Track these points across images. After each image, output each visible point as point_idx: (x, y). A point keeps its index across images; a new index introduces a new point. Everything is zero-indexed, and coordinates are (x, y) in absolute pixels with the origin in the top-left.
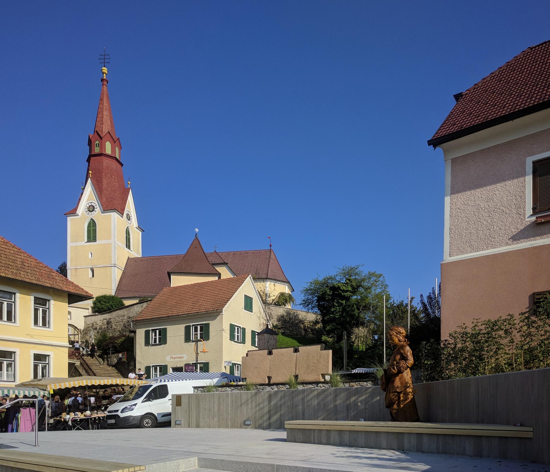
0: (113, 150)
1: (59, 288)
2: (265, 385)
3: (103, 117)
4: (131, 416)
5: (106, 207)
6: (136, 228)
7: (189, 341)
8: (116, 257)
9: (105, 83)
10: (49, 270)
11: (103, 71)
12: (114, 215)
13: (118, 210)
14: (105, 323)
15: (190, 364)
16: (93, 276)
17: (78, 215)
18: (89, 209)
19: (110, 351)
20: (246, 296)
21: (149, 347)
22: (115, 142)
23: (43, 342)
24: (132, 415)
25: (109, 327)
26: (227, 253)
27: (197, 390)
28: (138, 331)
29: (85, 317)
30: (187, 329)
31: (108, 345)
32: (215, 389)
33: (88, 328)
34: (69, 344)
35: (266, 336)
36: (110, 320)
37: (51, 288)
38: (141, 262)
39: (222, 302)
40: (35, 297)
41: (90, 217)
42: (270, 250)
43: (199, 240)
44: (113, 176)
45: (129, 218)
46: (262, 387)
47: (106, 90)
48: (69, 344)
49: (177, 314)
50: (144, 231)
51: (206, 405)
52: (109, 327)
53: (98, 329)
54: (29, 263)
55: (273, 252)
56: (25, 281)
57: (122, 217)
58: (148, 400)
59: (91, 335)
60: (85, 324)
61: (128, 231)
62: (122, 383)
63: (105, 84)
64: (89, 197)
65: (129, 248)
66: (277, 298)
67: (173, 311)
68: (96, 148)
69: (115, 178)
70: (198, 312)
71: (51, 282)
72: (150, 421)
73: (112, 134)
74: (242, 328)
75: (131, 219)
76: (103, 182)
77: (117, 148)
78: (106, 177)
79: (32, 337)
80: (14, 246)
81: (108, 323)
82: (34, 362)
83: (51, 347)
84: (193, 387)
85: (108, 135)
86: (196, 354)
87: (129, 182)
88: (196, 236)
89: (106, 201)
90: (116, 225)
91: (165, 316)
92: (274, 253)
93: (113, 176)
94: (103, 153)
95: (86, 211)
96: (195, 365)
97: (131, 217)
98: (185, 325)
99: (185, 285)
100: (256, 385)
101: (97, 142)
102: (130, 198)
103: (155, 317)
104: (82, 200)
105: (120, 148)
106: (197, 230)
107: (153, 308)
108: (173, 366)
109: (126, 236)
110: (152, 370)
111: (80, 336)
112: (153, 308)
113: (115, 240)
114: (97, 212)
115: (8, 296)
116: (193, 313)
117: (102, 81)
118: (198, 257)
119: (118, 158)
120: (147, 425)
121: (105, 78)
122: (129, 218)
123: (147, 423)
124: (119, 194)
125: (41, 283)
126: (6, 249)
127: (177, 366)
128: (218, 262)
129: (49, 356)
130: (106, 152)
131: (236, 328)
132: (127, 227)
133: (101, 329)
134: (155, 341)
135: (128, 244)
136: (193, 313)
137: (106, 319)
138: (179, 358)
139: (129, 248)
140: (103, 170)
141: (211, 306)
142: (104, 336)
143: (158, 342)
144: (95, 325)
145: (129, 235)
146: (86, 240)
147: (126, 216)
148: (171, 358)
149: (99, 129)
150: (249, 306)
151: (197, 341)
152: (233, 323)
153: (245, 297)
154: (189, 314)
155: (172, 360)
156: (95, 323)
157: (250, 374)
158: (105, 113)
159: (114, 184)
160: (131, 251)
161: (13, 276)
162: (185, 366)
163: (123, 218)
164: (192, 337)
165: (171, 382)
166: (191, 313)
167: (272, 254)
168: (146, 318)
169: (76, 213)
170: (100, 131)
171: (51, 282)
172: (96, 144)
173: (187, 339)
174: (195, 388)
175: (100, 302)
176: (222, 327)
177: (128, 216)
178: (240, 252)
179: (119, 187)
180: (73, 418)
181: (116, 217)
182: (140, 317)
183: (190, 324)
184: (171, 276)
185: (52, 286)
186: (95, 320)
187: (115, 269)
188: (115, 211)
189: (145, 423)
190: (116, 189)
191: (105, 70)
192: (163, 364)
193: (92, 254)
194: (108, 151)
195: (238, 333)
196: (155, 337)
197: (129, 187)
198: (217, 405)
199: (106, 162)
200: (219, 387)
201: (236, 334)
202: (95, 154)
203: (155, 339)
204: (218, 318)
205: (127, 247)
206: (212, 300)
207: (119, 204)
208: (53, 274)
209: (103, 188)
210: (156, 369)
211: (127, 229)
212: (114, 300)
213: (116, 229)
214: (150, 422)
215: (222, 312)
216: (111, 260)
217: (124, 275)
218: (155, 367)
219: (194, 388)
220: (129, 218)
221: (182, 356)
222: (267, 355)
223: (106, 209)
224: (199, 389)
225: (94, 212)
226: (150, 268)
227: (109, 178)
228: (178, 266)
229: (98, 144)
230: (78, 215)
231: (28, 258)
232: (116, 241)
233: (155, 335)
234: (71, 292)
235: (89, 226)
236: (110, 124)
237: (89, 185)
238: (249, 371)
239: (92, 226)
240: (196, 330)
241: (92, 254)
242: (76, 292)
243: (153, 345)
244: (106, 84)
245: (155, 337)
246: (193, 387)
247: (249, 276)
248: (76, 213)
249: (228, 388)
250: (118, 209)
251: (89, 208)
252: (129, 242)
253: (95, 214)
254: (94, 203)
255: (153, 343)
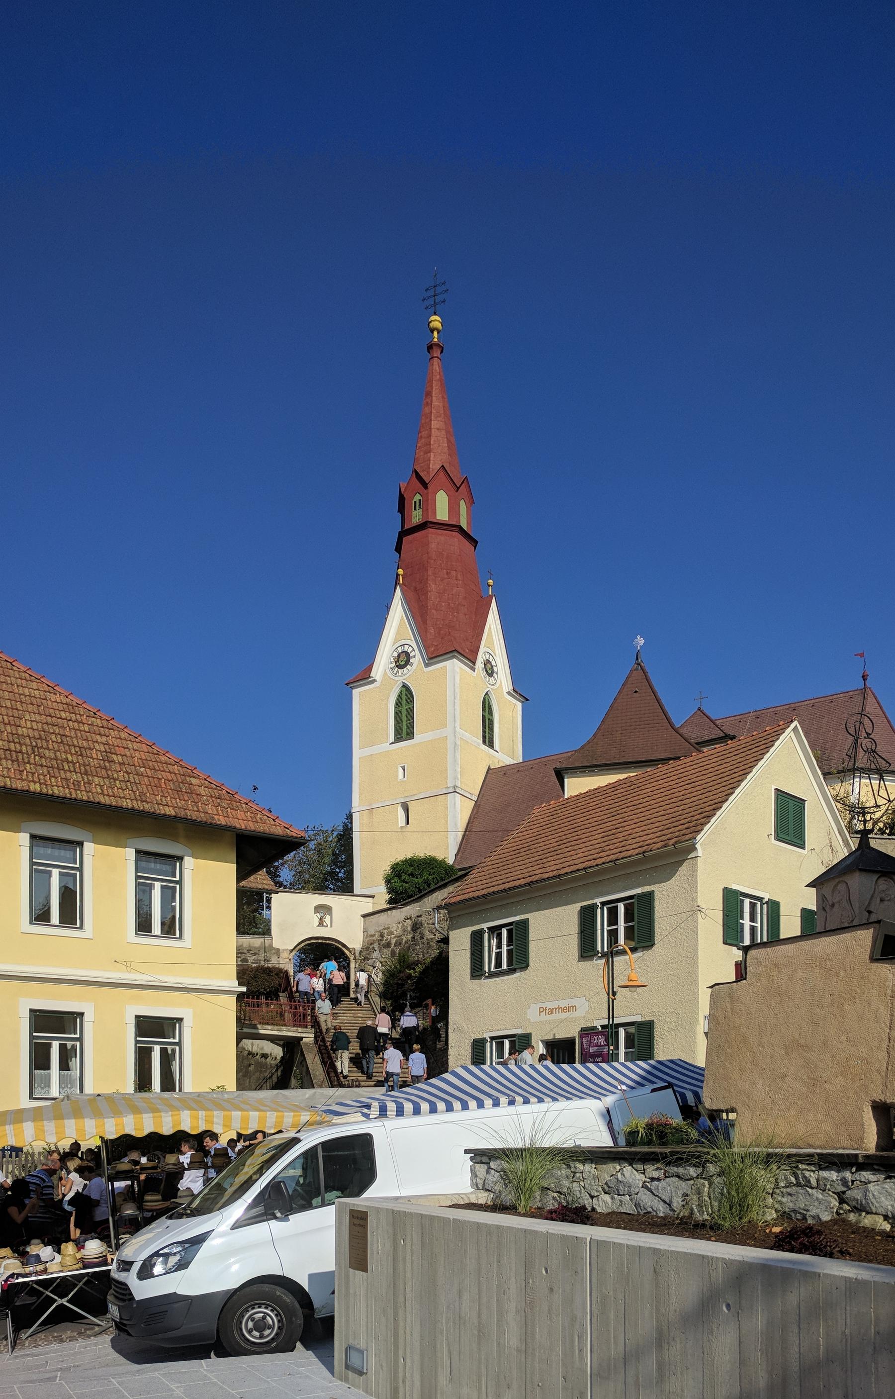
0: (453, 509)
1: (202, 817)
2: (861, 1167)
3: (430, 436)
4: (173, 1298)
5: (434, 650)
6: (509, 693)
7: (592, 953)
8: (459, 770)
9: (436, 352)
10: (182, 771)
11: (431, 324)
12: (454, 666)
13: (462, 653)
14: (409, 929)
15: (595, 1028)
16: (408, 823)
17: (375, 681)
18: (398, 664)
19: (406, 1000)
20: (780, 794)
21: (483, 981)
22: (455, 488)
23: (161, 981)
24: (182, 1291)
25: (416, 938)
26: (736, 718)
27: (486, 1167)
28: (454, 935)
29: (364, 916)
30: (587, 917)
31: (403, 985)
32: (564, 1172)
33: (371, 944)
34: (240, 985)
35: (857, 882)
36: (420, 919)
37: (176, 818)
38: (518, 775)
39: (694, 818)
40: (138, 852)
41: (400, 680)
42: (864, 691)
43: (647, 669)
44: (454, 573)
45: (489, 670)
46: (833, 1175)
47: (438, 369)
48: (240, 985)
49: (555, 873)
50: (527, 700)
51: (466, 1296)
52: (417, 937)
53: (393, 946)
54: (128, 754)
55: (873, 694)
56: (98, 803)
57: (473, 669)
58: (265, 1214)
59: (375, 961)
60: (364, 935)
61: (489, 704)
62: (202, 1127)
63: (435, 356)
64: (398, 633)
65: (491, 745)
66: (890, 812)
67: (547, 865)
68: (414, 513)
69: (456, 577)
70: (616, 860)
71: (181, 803)
72: (272, 1319)
73: (450, 471)
74: (767, 902)
75: (497, 673)
76: (430, 592)
77: (462, 503)
78: (436, 577)
79: (128, 966)
80: (95, 714)
81: (416, 927)
82: (137, 1042)
83: (185, 995)
84: (467, 1151)
85: (442, 474)
86: (608, 994)
87: (491, 582)
88: (637, 659)
89: (437, 635)
90: (458, 690)
91: (522, 882)
92: (876, 698)
93: (454, 573)
94: (430, 520)
95: (392, 669)
96: (610, 1031)
97: (495, 669)
98: (578, 906)
99: (590, 791)
100: (793, 1160)
101: (418, 497)
102: (493, 622)
103: (496, 889)
104: (384, 643)
105: (471, 502)
106: (640, 641)
107: (496, 866)
108: (546, 1037)
109: (484, 717)
110: (490, 1050)
111: (354, 966)
112: (496, 866)
113: (455, 727)
114: (414, 666)
115: (69, 854)
116: (603, 863)
117: (429, 352)
118: (642, 716)
119: (465, 527)
120: (257, 1334)
121: (436, 340)
122: (490, 672)
123: (260, 1326)
124: (466, 615)
125: (147, 807)
126: (70, 720)
127: (557, 1037)
128: (707, 738)
129: (180, 1020)
130: (437, 518)
131: (747, 902)
132: (487, 694)
133: (400, 944)
134: (498, 964)
135: (487, 735)
136: (603, 863)
137: (410, 918)
138: (563, 1010)
139: (491, 745)
140: (429, 561)
141: (658, 834)
142: (404, 962)
143: (505, 966)
144: (385, 935)
145: (491, 713)
146: (392, 739)
147: (483, 666)
148: (542, 1010)
149: (422, 465)
150: (791, 826)
151: (611, 954)
152: (735, 887)
153: (777, 798)
154: (591, 867)
155: (544, 1017)
156: (385, 931)
157: (760, 1086)
158: (435, 424)
159: (455, 591)
160: (496, 751)
161: (67, 790)
162: (581, 1037)
163: (474, 671)
164: (601, 943)
165: (392, 1123)
166: (597, 865)
167: (870, 700)
168: (471, 895)
169: (370, 677)
170: (423, 471)
171: (181, 803)
172: (415, 502)
173: (587, 950)
174: (478, 1159)
175: (399, 876)
176: (694, 899)
177: (489, 666)
178: (774, 709)
179: (465, 598)
180: (12, 1276)
181: (458, 670)
182: (457, 894)
183: (594, 901)
184: (566, 780)
185: (182, 813)
186: (387, 923)
187: (455, 797)
188: (454, 657)
189: (250, 1325)
190: (458, 604)
191: (436, 321)
192: (519, 1031)
193: (404, 770)
194: (442, 513)
195: (753, 919)
196: (498, 950)
197: (490, 594)
198: (517, 1311)
199: (435, 539)
200: (584, 1162)
201: (746, 922)
202: (413, 525)
203: (499, 955)
204: (683, 870)
205: (484, 742)
206: (664, 818)
207: (467, 639)
208: (193, 781)
209: (430, 604)
210: (500, 1046)
211: (484, 699)
212: (433, 869)
213: (458, 701)
214: (271, 1322)
215: (693, 848)
216: (446, 778)
217: (477, 812)
218: (499, 1040)
219: (472, 1159)
220: (490, 672)
221: (572, 1002)
222: (873, 960)
223: (433, 656)
224: (493, 1165)
225: (408, 667)
226: (538, 786)
227: (442, 580)
228: (585, 749)
229: (420, 500)
230: (375, 681)
231: (129, 742)
232: (458, 729)
233: (499, 946)
234: (238, 826)
235: (398, 703)
236: (447, 449)
237: (397, 602)
238: (749, 1065)
239: (406, 698)
240: (613, 919)
241: (404, 770)
242: (253, 828)
243: (492, 975)
244: (439, 355)
245: (498, 950)
246: (467, 1151)
247: (793, 726)
248: (370, 677)
249: (628, 1170)
250: (464, 651)
251: (398, 660)
252: (491, 729)
253: (411, 673)
254: (410, 646)
255: (493, 969)
